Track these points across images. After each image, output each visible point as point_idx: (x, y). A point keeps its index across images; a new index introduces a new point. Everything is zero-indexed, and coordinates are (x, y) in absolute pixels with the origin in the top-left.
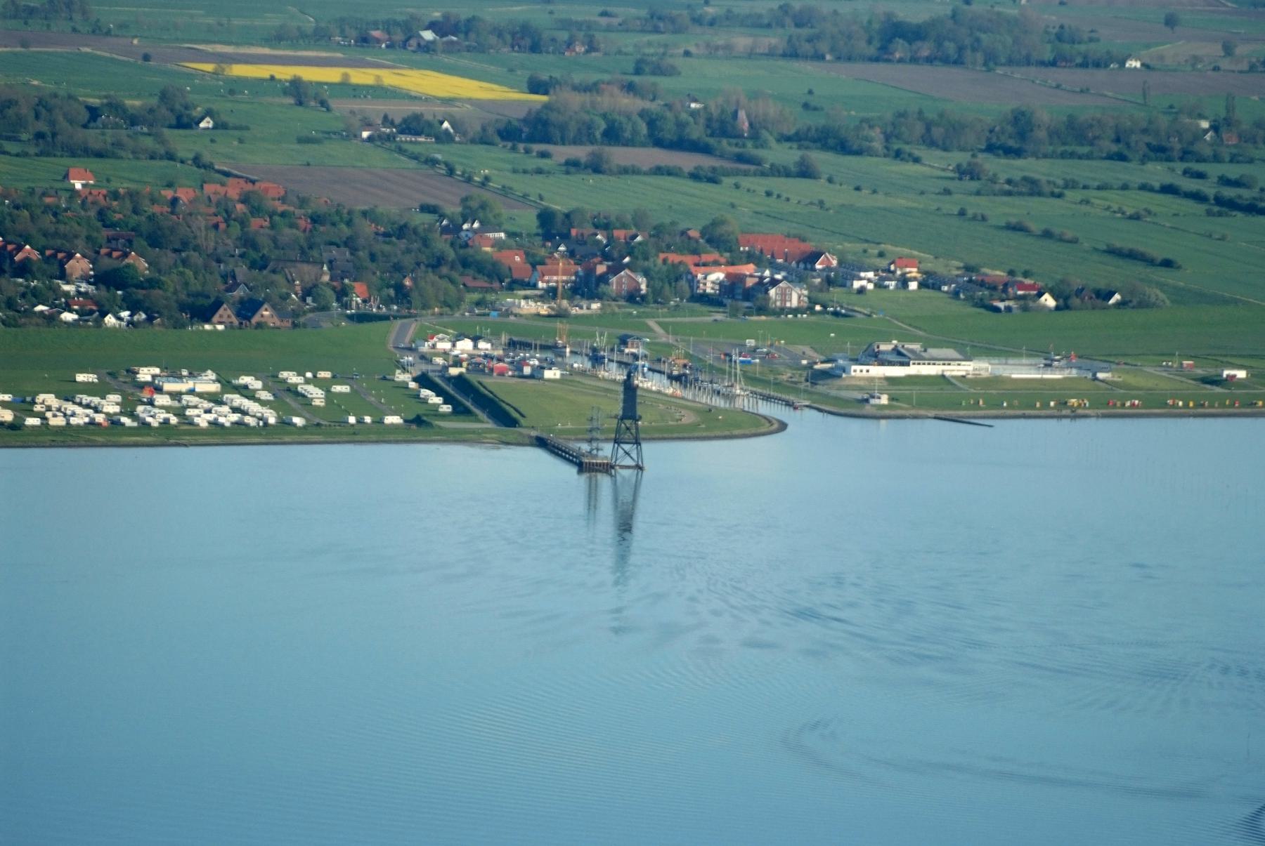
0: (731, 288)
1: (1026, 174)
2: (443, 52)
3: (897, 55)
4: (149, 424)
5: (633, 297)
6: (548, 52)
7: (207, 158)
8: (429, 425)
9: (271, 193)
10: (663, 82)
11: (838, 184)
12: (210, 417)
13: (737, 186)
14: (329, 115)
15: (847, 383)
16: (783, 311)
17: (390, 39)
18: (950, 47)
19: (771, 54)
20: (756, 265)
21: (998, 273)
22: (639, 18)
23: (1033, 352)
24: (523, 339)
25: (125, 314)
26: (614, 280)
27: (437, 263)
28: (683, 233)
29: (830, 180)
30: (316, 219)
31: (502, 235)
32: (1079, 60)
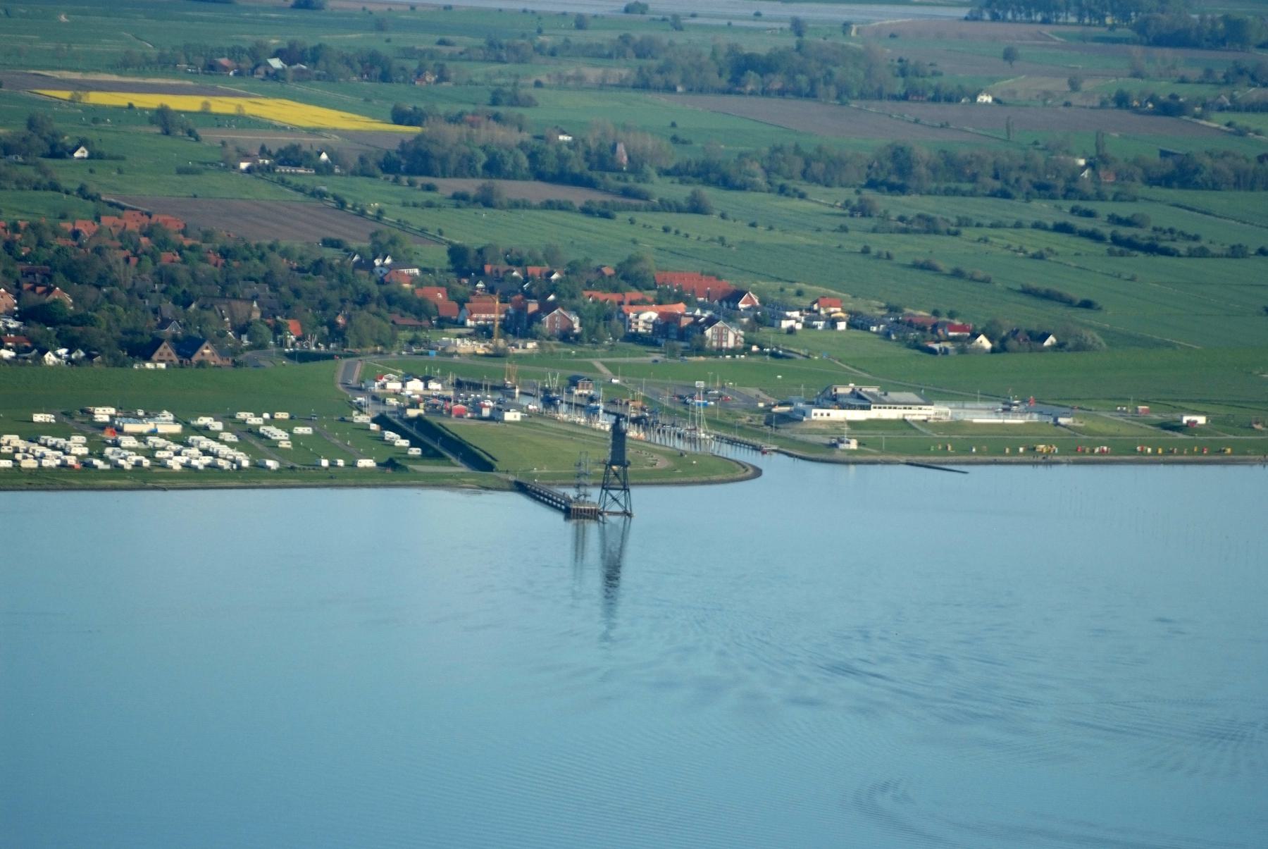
0: (665, 330)
1: (919, 212)
2: (294, 81)
3: (749, 88)
4: (122, 467)
5: (566, 336)
6: (398, 82)
7: (93, 189)
8: (403, 468)
9: (173, 225)
10: (528, 114)
11: (731, 221)
12: (183, 459)
13: (632, 222)
14: (196, 145)
15: (808, 426)
16: (720, 351)
17: (238, 67)
18: (803, 80)
19: (621, 86)
20: (686, 303)
21: (921, 313)
22: (481, 48)
23: (988, 396)
24: (470, 380)
25: (63, 351)
26: (547, 318)
27: (364, 300)
28: (599, 270)
29: (723, 216)
30: (226, 253)
31: (417, 271)
32: (931, 94)
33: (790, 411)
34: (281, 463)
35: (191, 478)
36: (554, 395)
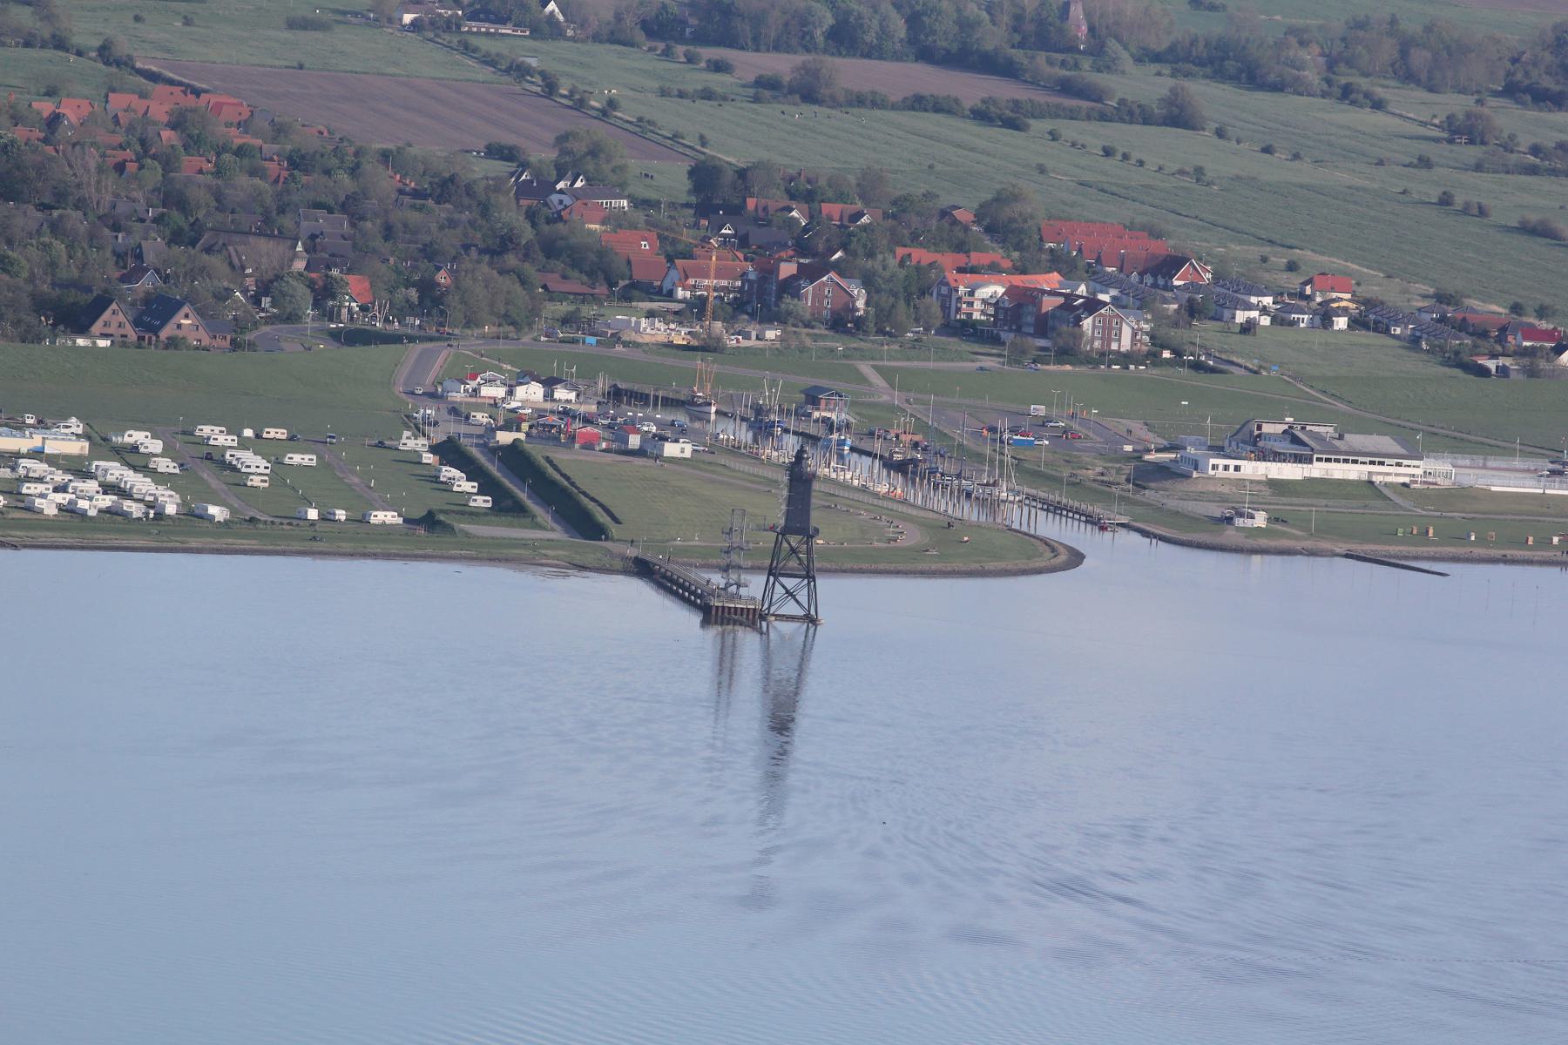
0: (1016, 313)
5: (842, 321)
7: (123, 47)
8: (448, 529)
13: (1054, 136)
15: (1200, 487)
16: (1105, 357)
21: (1494, 308)
23: (1532, 448)
28: (944, 214)
29: (1220, 133)
30: (298, 162)
31: (625, 203)
33: (1175, 461)
34: (233, 511)
35: (74, 530)
36: (774, 417)
